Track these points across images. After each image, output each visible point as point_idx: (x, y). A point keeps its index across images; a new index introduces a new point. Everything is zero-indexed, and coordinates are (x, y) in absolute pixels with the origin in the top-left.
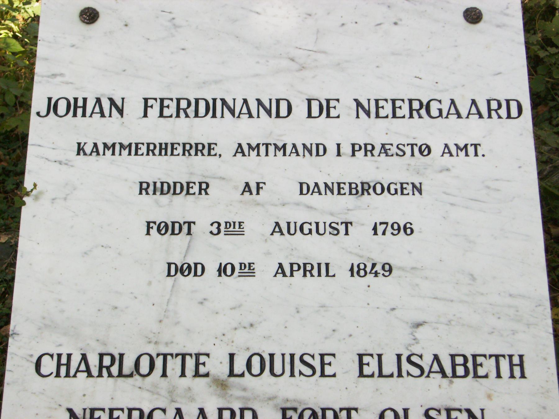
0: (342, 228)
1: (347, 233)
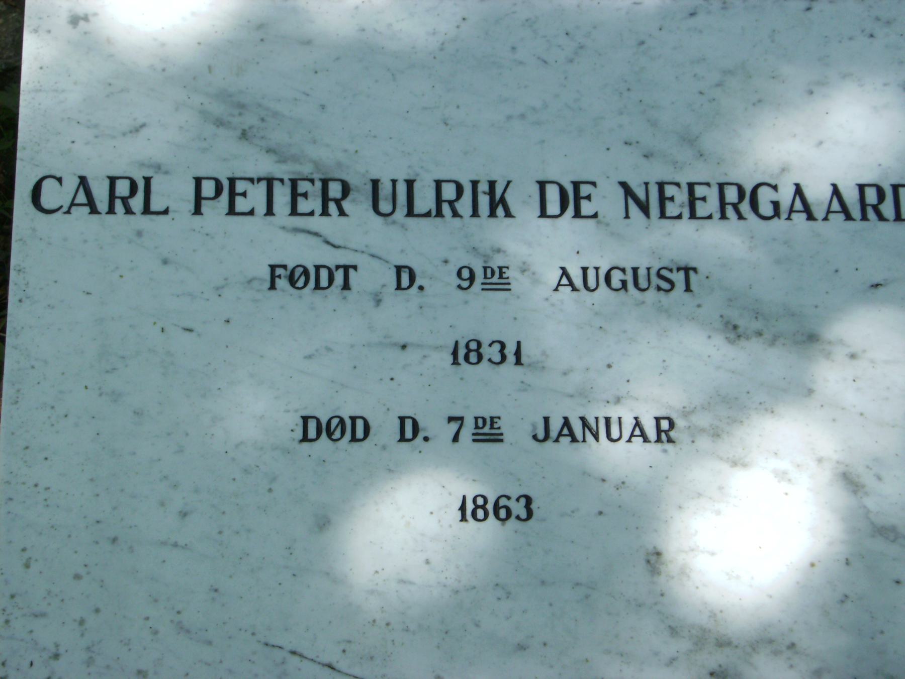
0: (678, 278)
1: (688, 289)
